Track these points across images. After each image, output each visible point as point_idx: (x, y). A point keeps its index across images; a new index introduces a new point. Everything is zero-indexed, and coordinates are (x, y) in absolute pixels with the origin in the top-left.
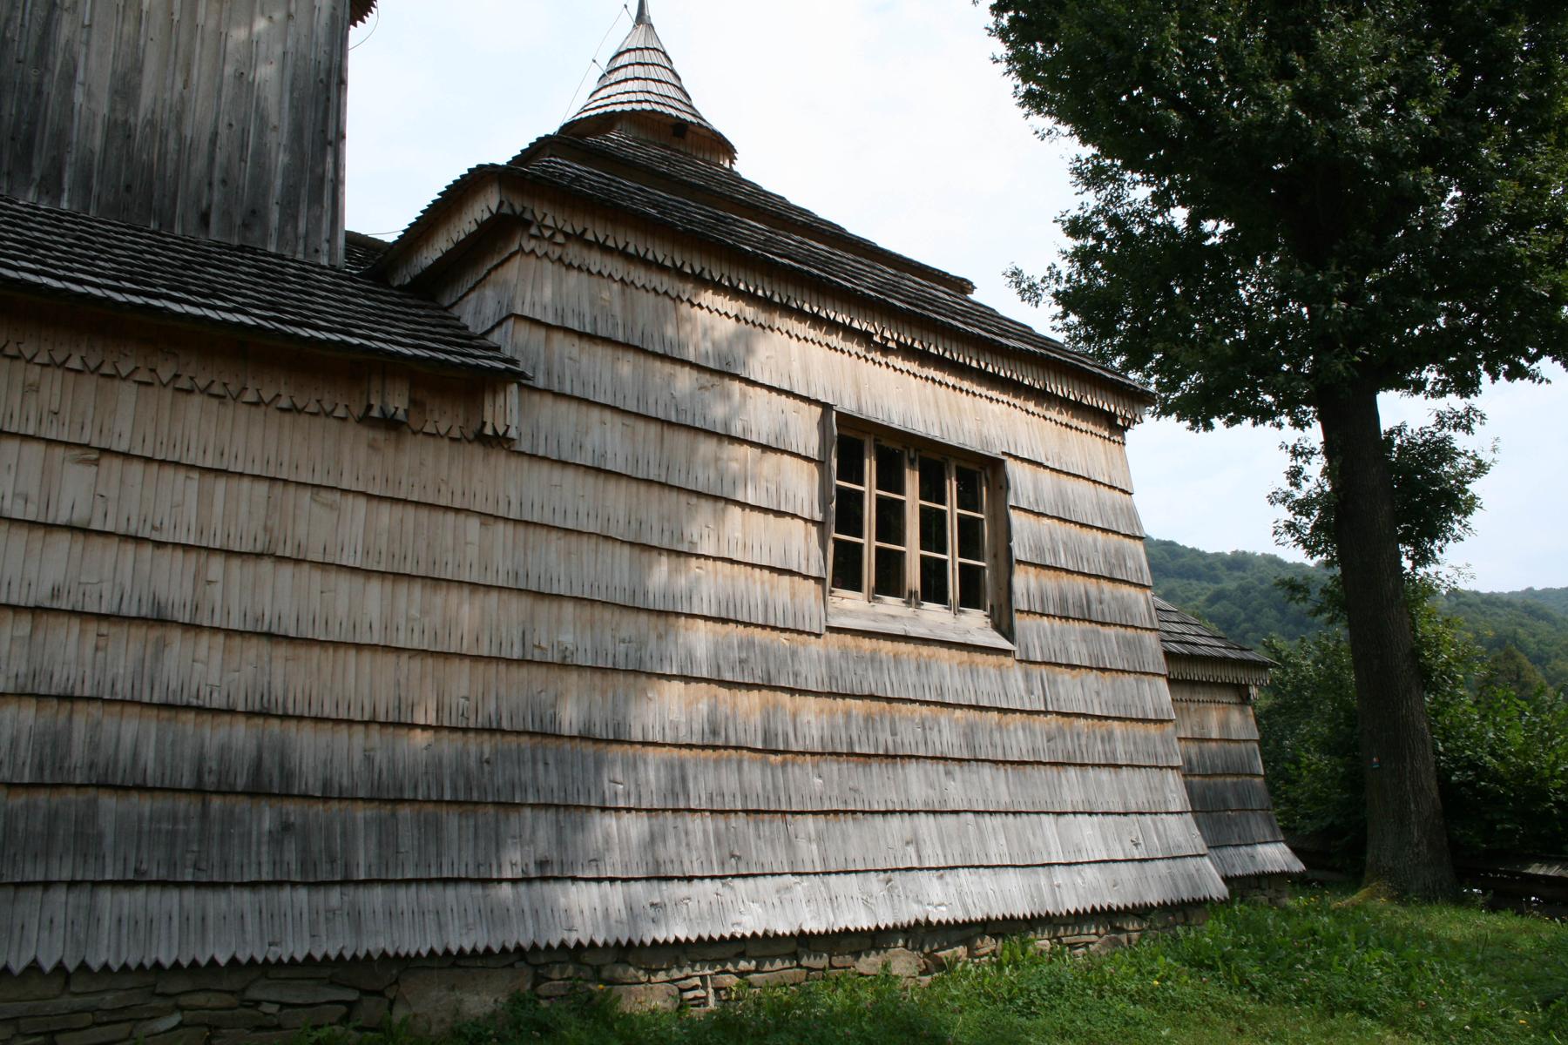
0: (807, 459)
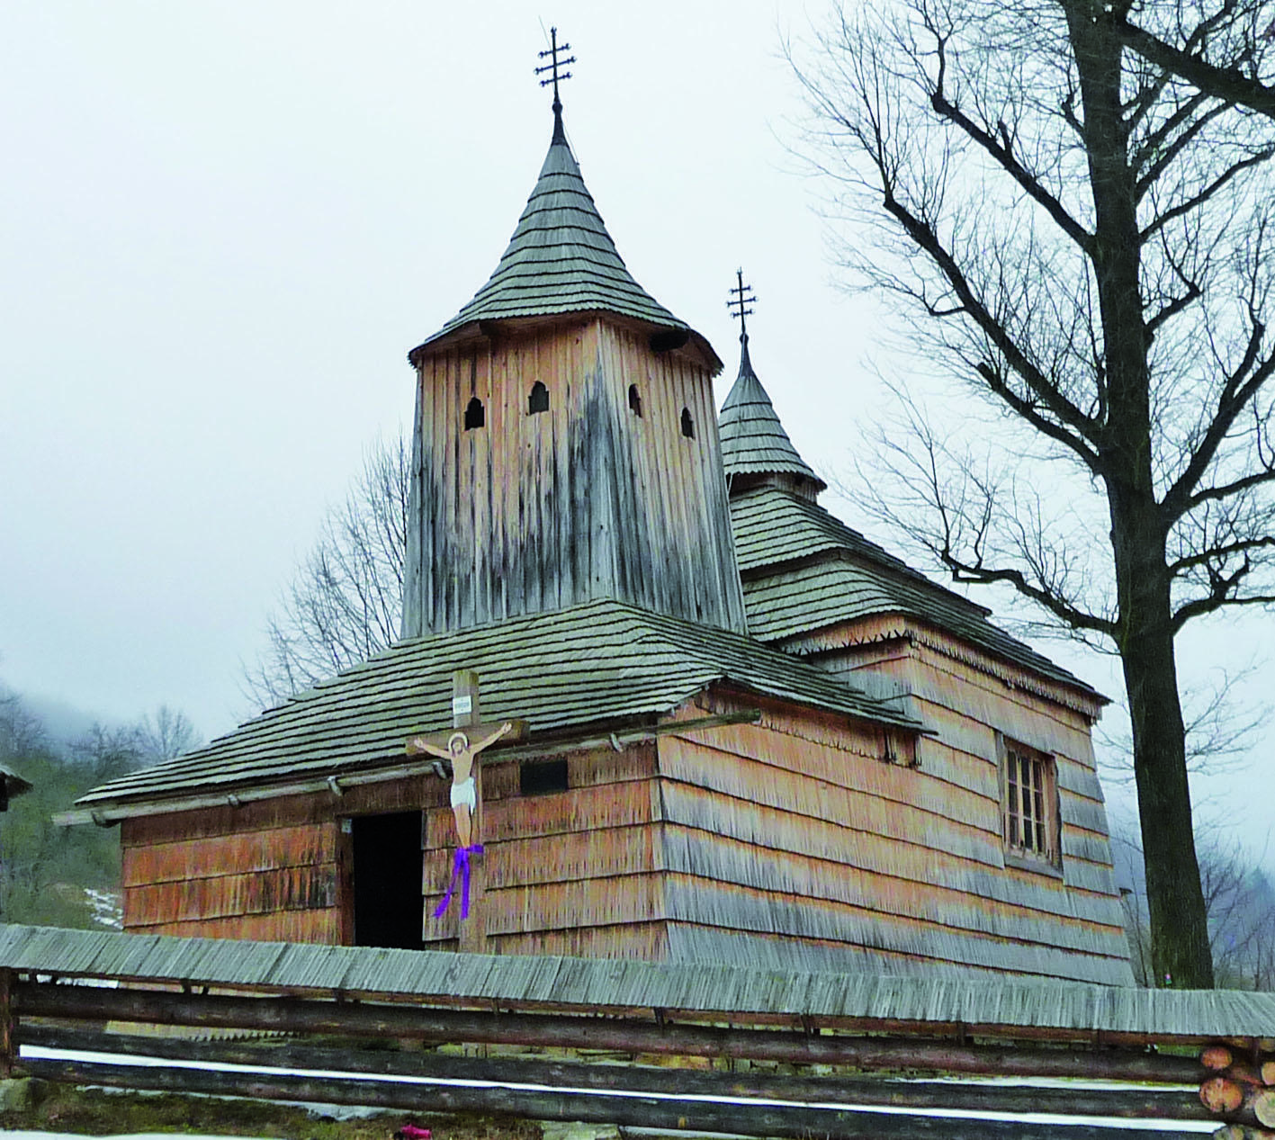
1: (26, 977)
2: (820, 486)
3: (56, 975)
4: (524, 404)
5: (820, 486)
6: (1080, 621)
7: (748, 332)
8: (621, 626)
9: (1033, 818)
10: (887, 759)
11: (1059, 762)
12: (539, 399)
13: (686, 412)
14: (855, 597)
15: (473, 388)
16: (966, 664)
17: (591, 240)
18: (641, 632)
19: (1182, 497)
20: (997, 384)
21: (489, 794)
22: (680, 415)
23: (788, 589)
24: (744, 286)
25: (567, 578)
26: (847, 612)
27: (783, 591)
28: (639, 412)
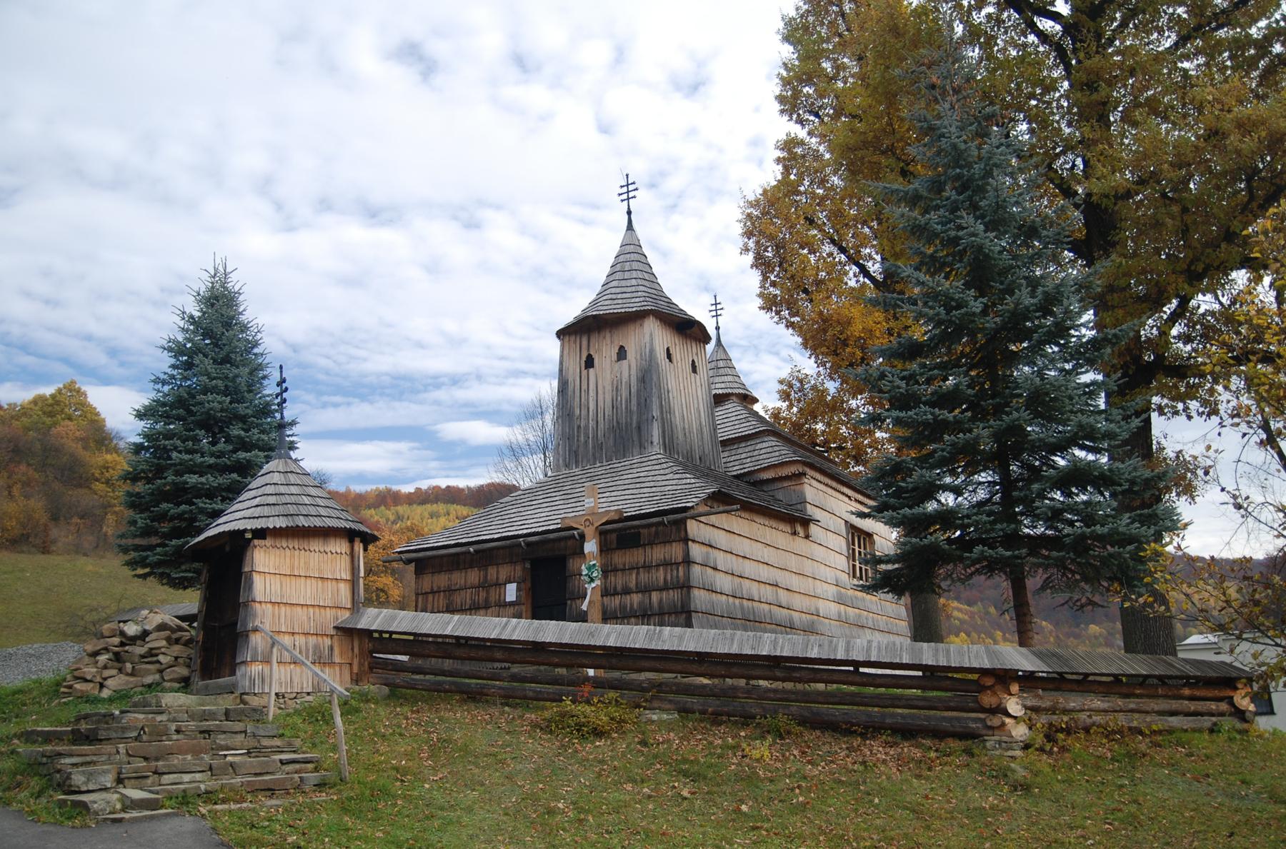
0: (694, 541)
1: (376, 635)
2: (755, 400)
3: (391, 633)
4: (615, 357)
5: (755, 400)
8: (665, 466)
10: (795, 533)
11: (875, 536)
12: (622, 355)
13: (693, 361)
14: (777, 454)
15: (588, 350)
16: (831, 487)
17: (647, 276)
18: (675, 469)
21: (604, 549)
23: (743, 451)
25: (636, 443)
26: (774, 461)
27: (740, 451)
28: (670, 361)
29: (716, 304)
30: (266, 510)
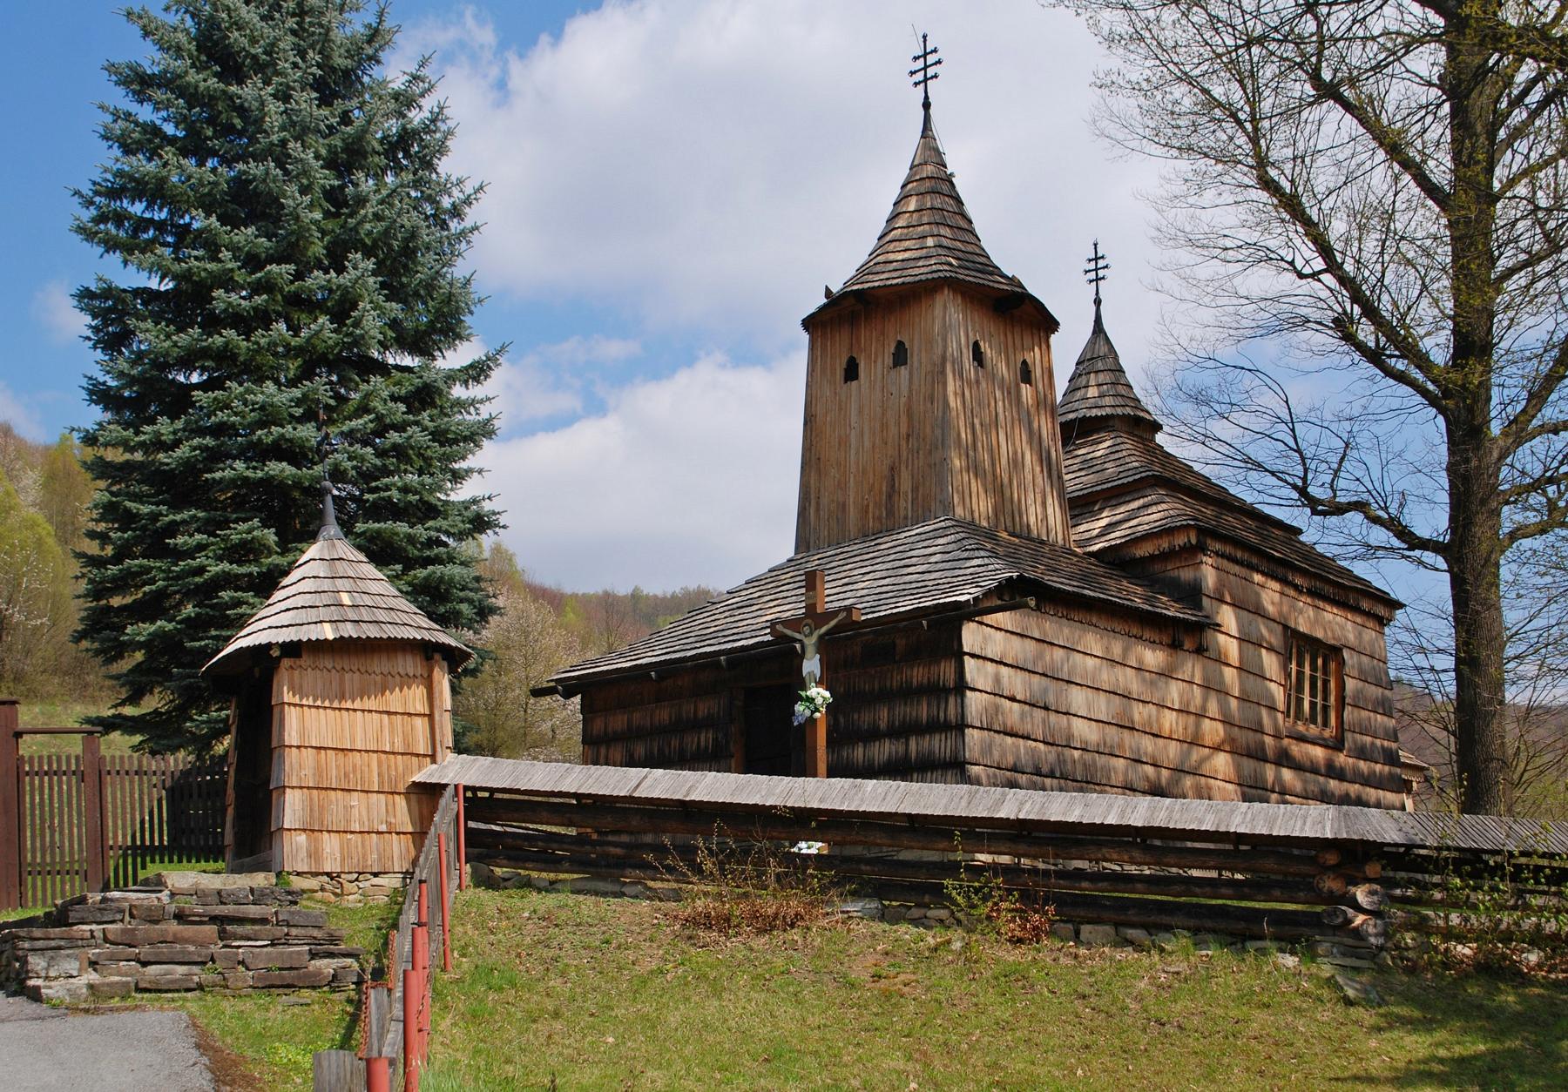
2: (1157, 427)
3: (492, 790)
4: (889, 360)
5: (1157, 427)
6: (1413, 542)
7: (1102, 295)
9: (1319, 700)
11: (1346, 654)
12: (900, 356)
19: (1519, 431)
20: (1349, 338)
22: (1019, 365)
24: (1099, 255)
29: (1096, 259)
30: (301, 616)
